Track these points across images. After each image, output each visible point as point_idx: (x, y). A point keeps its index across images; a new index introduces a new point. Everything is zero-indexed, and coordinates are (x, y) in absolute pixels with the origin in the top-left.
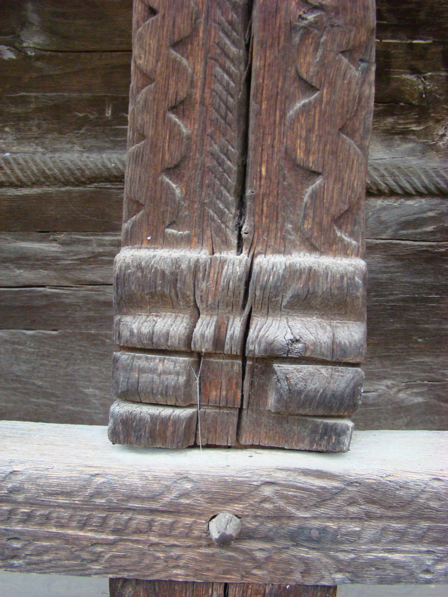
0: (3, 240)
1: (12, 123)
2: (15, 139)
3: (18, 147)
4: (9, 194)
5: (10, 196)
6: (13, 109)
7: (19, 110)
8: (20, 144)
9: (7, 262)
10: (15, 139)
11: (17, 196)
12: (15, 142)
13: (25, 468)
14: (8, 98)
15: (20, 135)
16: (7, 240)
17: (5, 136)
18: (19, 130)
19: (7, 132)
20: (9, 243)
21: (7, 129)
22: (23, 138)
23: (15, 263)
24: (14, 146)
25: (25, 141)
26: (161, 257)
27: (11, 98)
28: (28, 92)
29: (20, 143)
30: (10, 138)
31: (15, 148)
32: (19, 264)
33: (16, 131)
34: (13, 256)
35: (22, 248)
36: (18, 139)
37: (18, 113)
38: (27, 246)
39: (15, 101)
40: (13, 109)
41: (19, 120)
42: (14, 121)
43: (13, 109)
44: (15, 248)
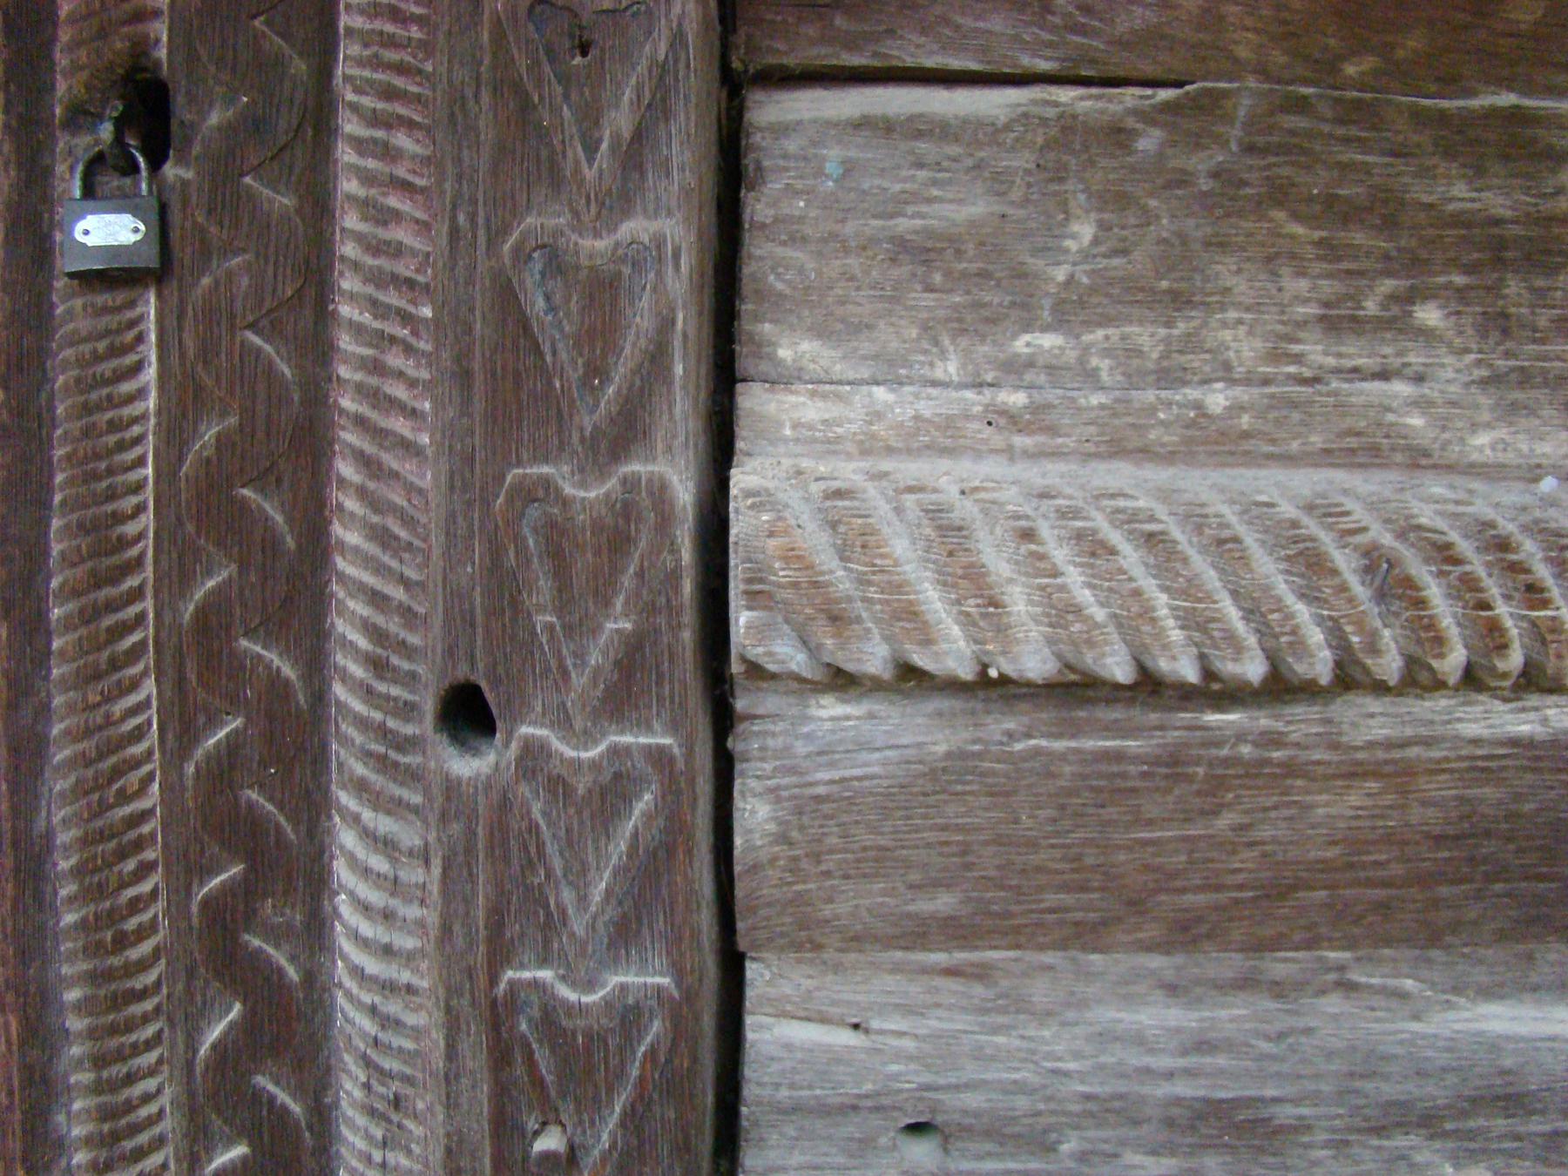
0: (1378, 1001)
1: (1459, 280)
2: (1483, 383)
3: (1502, 433)
4: (1471, 730)
5: (1476, 742)
6: (1460, 189)
7: (1497, 203)
8: (1511, 412)
9: (1403, 1126)
10: (1483, 383)
11: (1514, 742)
12: (1485, 401)
13: (284, 580)
14: (1419, 118)
15: (1507, 355)
16: (1402, 995)
17: (1415, 359)
18: (1499, 324)
19: (1427, 335)
20: (1416, 1017)
21: (1429, 315)
22: (1525, 378)
23: (1445, 1135)
24: (1474, 427)
25: (1541, 394)
26: (983, 566)
27: (1443, 117)
28: (1528, 89)
29: (1514, 407)
30: (1452, 373)
31: (1482, 439)
32: (1471, 1135)
33: (1483, 333)
34: (1436, 1092)
35: (1495, 1045)
36: (1494, 380)
37: (1498, 222)
38: (1523, 1029)
39: (1467, 142)
40: (1458, 193)
41: (1499, 262)
42: (1469, 269)
43: (1458, 193)
44: (1451, 1046)
